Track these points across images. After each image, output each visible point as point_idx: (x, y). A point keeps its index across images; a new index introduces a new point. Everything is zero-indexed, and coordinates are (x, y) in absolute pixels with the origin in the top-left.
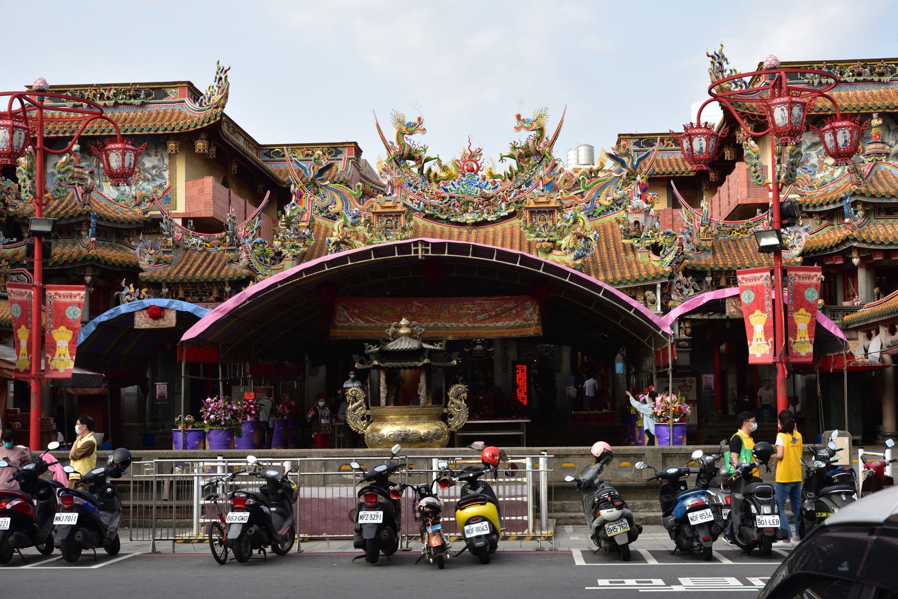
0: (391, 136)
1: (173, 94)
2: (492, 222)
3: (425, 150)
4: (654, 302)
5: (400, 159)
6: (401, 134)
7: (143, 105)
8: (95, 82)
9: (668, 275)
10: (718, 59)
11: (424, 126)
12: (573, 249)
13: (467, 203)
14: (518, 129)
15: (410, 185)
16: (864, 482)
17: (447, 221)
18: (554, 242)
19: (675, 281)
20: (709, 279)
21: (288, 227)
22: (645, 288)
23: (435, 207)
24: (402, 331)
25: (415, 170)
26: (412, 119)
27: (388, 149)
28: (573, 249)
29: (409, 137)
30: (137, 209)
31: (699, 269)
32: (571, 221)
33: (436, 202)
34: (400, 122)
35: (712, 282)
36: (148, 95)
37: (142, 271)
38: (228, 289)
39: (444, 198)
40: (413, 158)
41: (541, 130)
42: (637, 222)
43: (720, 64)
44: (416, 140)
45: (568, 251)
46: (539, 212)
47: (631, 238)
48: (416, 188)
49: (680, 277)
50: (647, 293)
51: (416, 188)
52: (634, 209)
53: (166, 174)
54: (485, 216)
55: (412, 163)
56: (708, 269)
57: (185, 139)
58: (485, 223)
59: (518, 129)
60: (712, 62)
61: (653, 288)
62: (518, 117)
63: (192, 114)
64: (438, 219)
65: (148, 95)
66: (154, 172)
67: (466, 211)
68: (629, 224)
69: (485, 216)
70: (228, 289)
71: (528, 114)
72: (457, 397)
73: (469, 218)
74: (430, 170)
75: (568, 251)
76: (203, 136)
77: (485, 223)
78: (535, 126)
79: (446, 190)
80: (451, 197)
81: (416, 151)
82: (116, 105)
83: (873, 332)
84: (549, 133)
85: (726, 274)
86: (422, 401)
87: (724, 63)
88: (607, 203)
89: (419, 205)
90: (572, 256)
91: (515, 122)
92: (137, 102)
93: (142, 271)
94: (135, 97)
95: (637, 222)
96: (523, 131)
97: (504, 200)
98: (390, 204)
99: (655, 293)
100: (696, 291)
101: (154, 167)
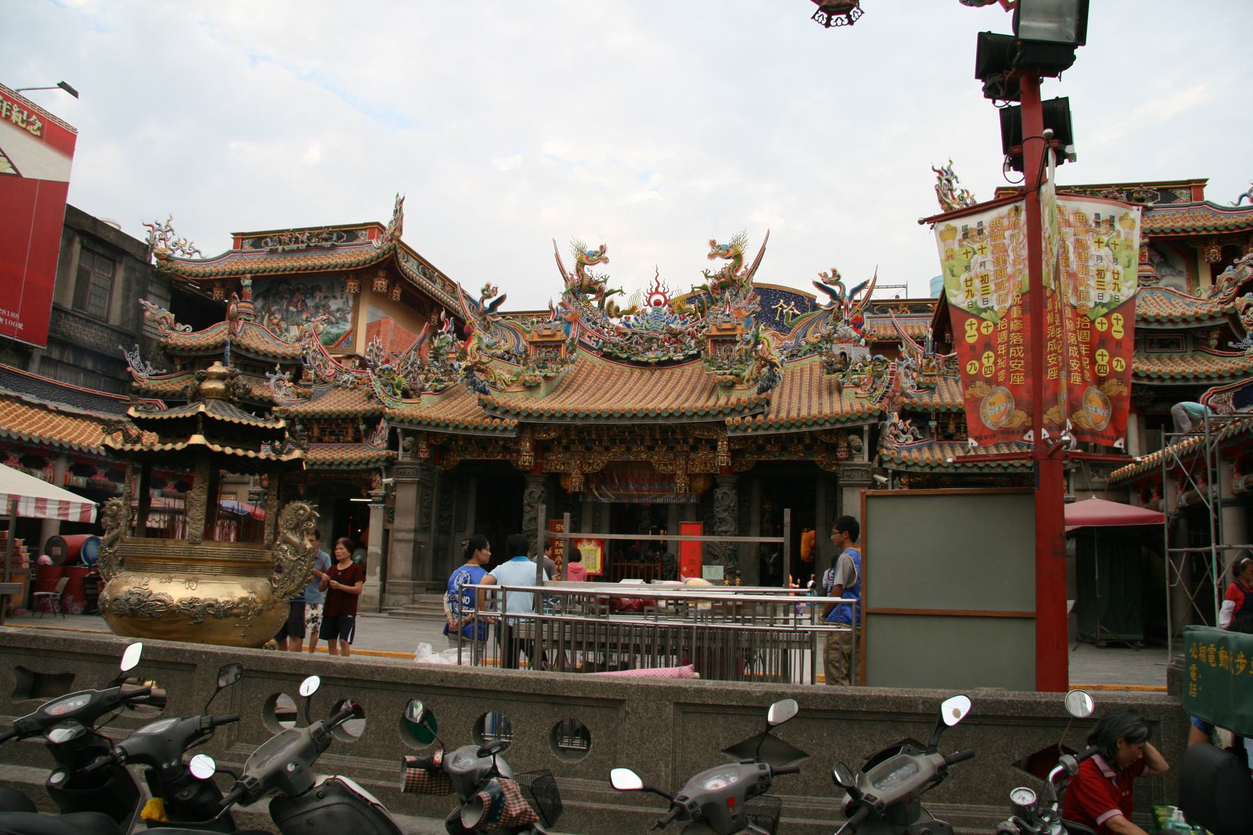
0: (570, 268)
1: (363, 236)
2: (678, 362)
3: (605, 281)
4: (859, 450)
5: (580, 291)
6: (581, 265)
7: (333, 247)
8: (291, 227)
9: (877, 414)
10: (945, 178)
11: (606, 255)
12: (756, 380)
13: (650, 340)
14: (711, 256)
15: (589, 320)
16: (813, 462)
17: (628, 361)
18: (737, 375)
19: (888, 423)
20: (933, 424)
21: (436, 359)
22: (850, 431)
23: (614, 345)
24: (208, 385)
25: (595, 304)
26: (593, 247)
27: (566, 279)
28: (756, 380)
29: (591, 268)
30: (297, 344)
31: (919, 410)
32: (752, 342)
33: (618, 339)
34: (581, 251)
35: (937, 428)
36: (340, 238)
37: (276, 405)
38: (362, 427)
39: (625, 334)
40: (593, 292)
41: (738, 257)
42: (843, 354)
43: (948, 181)
44: (595, 271)
45: (751, 382)
46: (724, 342)
47: (835, 372)
48: (595, 323)
49: (895, 417)
50: (852, 437)
51: (595, 323)
52: (839, 339)
53: (349, 317)
54: (671, 354)
55: (592, 296)
56: (931, 410)
57: (363, 274)
58: (670, 363)
59: (711, 256)
60: (939, 179)
61: (859, 431)
62: (713, 243)
63: (373, 248)
64: (616, 359)
65: (340, 238)
66: (338, 315)
67: (649, 349)
68: (834, 356)
69: (671, 354)
70: (362, 427)
71: (724, 240)
72: (296, 528)
73: (651, 356)
74: (611, 303)
75: (751, 382)
76: (381, 274)
77: (670, 363)
78: (732, 252)
79: (628, 326)
80: (634, 334)
81: (597, 282)
82: (309, 248)
83: (1154, 491)
84: (748, 260)
85: (955, 419)
86: (217, 538)
87: (954, 182)
88: (815, 340)
89: (597, 342)
90: (755, 389)
91: (709, 250)
92: (328, 244)
93: (276, 405)
94: (326, 240)
95: (843, 354)
96: (718, 259)
97: (693, 336)
98: (548, 332)
99: (862, 439)
100: (916, 439)
101: (338, 310)
